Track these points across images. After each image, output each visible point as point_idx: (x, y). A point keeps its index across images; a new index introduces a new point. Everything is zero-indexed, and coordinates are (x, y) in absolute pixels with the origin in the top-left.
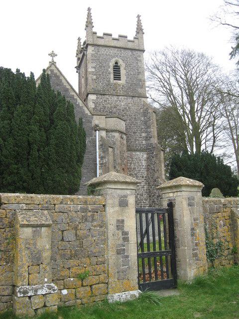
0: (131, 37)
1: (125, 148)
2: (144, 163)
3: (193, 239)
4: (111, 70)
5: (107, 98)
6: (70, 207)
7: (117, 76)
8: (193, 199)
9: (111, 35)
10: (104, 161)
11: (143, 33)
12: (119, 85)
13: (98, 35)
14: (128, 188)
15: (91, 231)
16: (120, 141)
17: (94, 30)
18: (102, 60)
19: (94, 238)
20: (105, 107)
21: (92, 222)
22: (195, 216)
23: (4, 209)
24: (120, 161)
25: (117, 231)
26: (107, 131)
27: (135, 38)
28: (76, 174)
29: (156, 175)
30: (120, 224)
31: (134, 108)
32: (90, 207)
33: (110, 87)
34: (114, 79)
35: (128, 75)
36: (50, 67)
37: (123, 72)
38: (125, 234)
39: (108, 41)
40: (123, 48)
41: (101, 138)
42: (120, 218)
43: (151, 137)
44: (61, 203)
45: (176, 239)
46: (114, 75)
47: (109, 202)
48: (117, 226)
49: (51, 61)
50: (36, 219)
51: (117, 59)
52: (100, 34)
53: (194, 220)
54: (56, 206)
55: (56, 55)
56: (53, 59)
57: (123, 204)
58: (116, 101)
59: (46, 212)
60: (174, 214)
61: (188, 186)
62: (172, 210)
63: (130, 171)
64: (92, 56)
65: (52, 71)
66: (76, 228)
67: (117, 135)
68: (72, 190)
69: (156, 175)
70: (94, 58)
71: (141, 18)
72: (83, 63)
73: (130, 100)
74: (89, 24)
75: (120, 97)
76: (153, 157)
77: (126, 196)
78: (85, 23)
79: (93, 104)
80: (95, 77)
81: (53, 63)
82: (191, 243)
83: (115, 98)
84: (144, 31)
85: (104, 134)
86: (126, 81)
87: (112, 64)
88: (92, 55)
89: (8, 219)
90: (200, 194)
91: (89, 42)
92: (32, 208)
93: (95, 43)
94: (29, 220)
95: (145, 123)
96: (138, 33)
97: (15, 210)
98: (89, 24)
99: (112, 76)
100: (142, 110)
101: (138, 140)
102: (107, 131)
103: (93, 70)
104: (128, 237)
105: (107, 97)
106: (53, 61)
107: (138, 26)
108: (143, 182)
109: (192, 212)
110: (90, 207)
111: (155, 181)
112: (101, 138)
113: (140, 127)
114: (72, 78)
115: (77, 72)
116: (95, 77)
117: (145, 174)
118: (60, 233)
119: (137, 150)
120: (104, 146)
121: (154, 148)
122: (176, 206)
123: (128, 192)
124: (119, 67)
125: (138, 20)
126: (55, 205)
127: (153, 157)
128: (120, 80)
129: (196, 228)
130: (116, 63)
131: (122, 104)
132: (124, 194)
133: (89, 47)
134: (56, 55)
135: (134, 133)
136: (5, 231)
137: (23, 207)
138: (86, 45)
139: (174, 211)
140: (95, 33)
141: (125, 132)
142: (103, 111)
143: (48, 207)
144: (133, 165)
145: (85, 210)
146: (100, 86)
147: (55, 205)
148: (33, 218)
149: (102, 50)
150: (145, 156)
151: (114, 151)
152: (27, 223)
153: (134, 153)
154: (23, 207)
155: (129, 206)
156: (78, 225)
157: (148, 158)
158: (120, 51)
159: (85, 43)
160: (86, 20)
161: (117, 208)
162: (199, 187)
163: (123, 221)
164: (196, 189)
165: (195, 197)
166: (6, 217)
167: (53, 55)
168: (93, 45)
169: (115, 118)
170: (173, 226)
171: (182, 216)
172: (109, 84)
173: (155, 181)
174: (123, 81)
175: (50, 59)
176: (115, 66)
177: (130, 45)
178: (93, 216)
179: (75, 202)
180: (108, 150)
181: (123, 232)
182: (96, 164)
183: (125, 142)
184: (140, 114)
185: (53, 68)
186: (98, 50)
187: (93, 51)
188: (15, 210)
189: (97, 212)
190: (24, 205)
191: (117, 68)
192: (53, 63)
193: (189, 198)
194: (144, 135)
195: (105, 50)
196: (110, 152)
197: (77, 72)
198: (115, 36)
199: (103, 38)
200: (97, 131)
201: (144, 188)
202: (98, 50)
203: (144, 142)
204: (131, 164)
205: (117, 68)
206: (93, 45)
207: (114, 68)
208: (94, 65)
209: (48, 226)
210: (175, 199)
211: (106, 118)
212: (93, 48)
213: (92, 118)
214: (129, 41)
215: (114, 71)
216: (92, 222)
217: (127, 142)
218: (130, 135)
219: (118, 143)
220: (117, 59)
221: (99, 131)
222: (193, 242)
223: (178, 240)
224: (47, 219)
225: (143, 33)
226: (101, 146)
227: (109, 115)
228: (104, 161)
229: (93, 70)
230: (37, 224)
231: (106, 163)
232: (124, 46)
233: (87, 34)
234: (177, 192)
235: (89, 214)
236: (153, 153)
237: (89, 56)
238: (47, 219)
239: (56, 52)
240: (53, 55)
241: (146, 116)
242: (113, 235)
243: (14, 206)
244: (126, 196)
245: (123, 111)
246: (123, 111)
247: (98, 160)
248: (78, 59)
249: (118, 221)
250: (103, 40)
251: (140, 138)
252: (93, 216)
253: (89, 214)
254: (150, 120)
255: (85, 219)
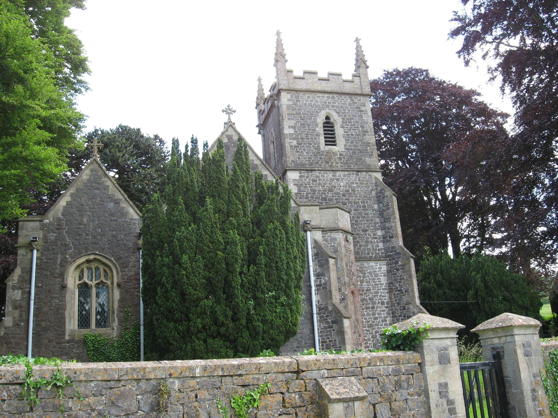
0: (348, 75)
1: (352, 257)
2: (384, 280)
3: (535, 405)
4: (320, 130)
5: (317, 177)
6: (379, 370)
7: (331, 140)
8: (530, 346)
9: (315, 73)
10: (323, 281)
11: (367, 67)
12: (335, 154)
13: (296, 74)
14: (449, 336)
15: (409, 402)
16: (345, 246)
17: (288, 66)
18: (303, 114)
19: (413, 412)
20: (314, 191)
21: (407, 389)
22: (535, 371)
23: (302, 379)
24: (347, 279)
25: (441, 400)
26: (324, 231)
27: (354, 76)
28: (294, 308)
29: (405, 299)
30: (443, 388)
31: (360, 191)
32: (403, 368)
33: (321, 158)
34: (326, 145)
35: (347, 137)
36: (227, 130)
37: (339, 132)
38: (450, 402)
39: (312, 83)
40: (336, 93)
41: (316, 243)
42: (442, 381)
43: (392, 237)
44: (369, 364)
45: (510, 406)
46: (325, 138)
47: (427, 358)
48: (440, 393)
49: (226, 121)
50: (346, 390)
51: (327, 110)
52: (298, 73)
53: (534, 377)
54: (364, 369)
55: (234, 111)
56: (229, 118)
57: (444, 360)
58: (332, 180)
59: (353, 378)
60: (504, 369)
61: (521, 326)
62: (500, 363)
63: (361, 295)
64: (288, 109)
65: (230, 137)
66: (390, 401)
67: (340, 236)
68: (276, 337)
69: (405, 299)
70: (291, 111)
71: (361, 43)
72: (270, 120)
73: (353, 177)
74: (280, 57)
75: (338, 174)
76: (398, 270)
77: (446, 349)
78: (274, 56)
79: (296, 187)
80: (295, 143)
81: (230, 125)
82: (533, 411)
83: (330, 175)
84: (368, 63)
85: (318, 235)
86: (345, 146)
87: (321, 120)
88: (288, 107)
89: (308, 393)
90: (537, 337)
91: (281, 87)
92: (335, 375)
93: (292, 86)
94: (339, 393)
95: (381, 213)
96: (358, 67)
97: (315, 379)
98: (280, 57)
99: (322, 139)
100: (374, 193)
101: (371, 242)
102: (324, 231)
103: (292, 131)
104: (455, 408)
105: (317, 173)
106: (230, 122)
107: (357, 56)
108: (383, 311)
109: (529, 365)
110: (403, 368)
111: (404, 309)
112: (316, 243)
113: (372, 220)
114: (256, 143)
115: (259, 133)
116: (295, 143)
117: (386, 299)
118: (372, 407)
119: (370, 259)
120: (322, 257)
121: (399, 254)
122: (506, 357)
123: (448, 342)
124: (332, 124)
125: (357, 47)
126: (361, 368)
127: (398, 270)
128: (335, 145)
129: (537, 389)
130: (327, 118)
131: (342, 184)
132: (443, 345)
133: (283, 94)
134: (234, 111)
135: (365, 231)
136: (306, 410)
137: (324, 374)
138: (277, 92)
139: (503, 365)
140: (291, 72)
141: (350, 230)
142: (312, 197)
143: (353, 372)
144: (365, 284)
145: (397, 372)
146: (304, 157)
147: (361, 368)
148: (342, 390)
149: (304, 99)
150: (384, 268)
151: (336, 263)
152: (338, 397)
153: (365, 264)
154: (324, 374)
155: (451, 362)
156: (392, 395)
157: (389, 271)
158: (333, 98)
159: (273, 88)
160: (275, 51)
161: (437, 367)
162: (535, 326)
163: (446, 384)
164: (531, 331)
165: (532, 342)
166: (306, 390)
167: (229, 111)
168: (289, 90)
169: (334, 209)
170: (504, 387)
171: (517, 371)
172: (318, 152)
173: (404, 309)
174: (340, 147)
175: (225, 118)
176: (327, 123)
177: (348, 88)
178: (408, 380)
179: (386, 362)
180: (327, 262)
181: (448, 401)
182: (310, 286)
183: (352, 247)
184: (370, 200)
185: (231, 132)
186: (297, 98)
187: (288, 100)
188: (315, 379)
189: (412, 374)
190: (325, 371)
191: (328, 125)
192: (230, 125)
193: (523, 345)
194: (379, 233)
195: (309, 97)
196: (331, 266)
197: (259, 133)
198: (323, 74)
199: (304, 78)
200: (308, 233)
201: (386, 321)
202: (297, 98)
203: (381, 245)
204: (362, 282)
205: (328, 125)
206: (289, 90)
207: (324, 127)
208: (292, 123)
209: (362, 399)
210: (503, 347)
211: (320, 209)
212: (289, 95)
213: (299, 210)
214: (344, 81)
215: (324, 130)
216: (407, 389)
217: (355, 246)
218: (357, 234)
219: (343, 250)
220: (327, 110)
221: (310, 231)
222: (535, 410)
223: (514, 408)
224: (359, 389)
225: (367, 67)
226: (316, 255)
227: (325, 203)
228: (323, 281)
229: (292, 131)
230: (351, 398)
231: (325, 284)
232: (339, 91)
233: (278, 74)
234: (506, 336)
235: (404, 377)
236: (397, 263)
237: (284, 109)
238: (359, 389)
239: (233, 107)
240: (229, 111)
241: (381, 203)
242: (436, 406)
243: (315, 374)
244: (446, 349)
245: (344, 195)
246: (344, 195)
247: (313, 278)
248: (261, 112)
249: (440, 385)
250: (304, 81)
251: (376, 238)
252: (408, 380)
253: (404, 377)
254: (388, 209)
255: (398, 385)
